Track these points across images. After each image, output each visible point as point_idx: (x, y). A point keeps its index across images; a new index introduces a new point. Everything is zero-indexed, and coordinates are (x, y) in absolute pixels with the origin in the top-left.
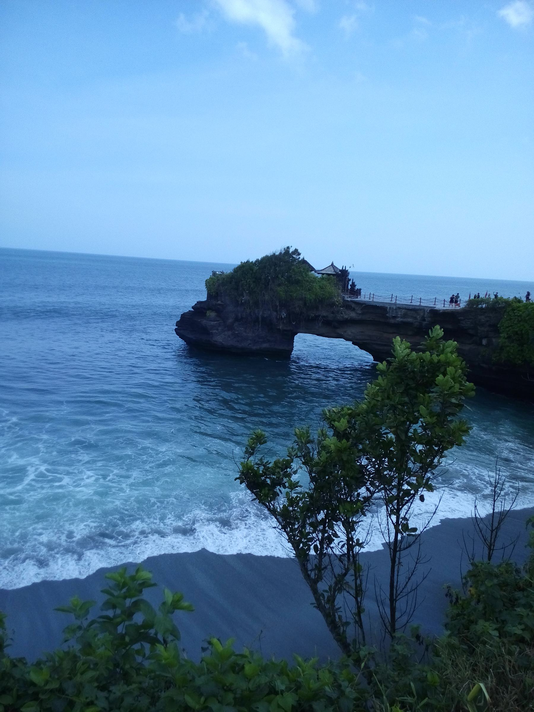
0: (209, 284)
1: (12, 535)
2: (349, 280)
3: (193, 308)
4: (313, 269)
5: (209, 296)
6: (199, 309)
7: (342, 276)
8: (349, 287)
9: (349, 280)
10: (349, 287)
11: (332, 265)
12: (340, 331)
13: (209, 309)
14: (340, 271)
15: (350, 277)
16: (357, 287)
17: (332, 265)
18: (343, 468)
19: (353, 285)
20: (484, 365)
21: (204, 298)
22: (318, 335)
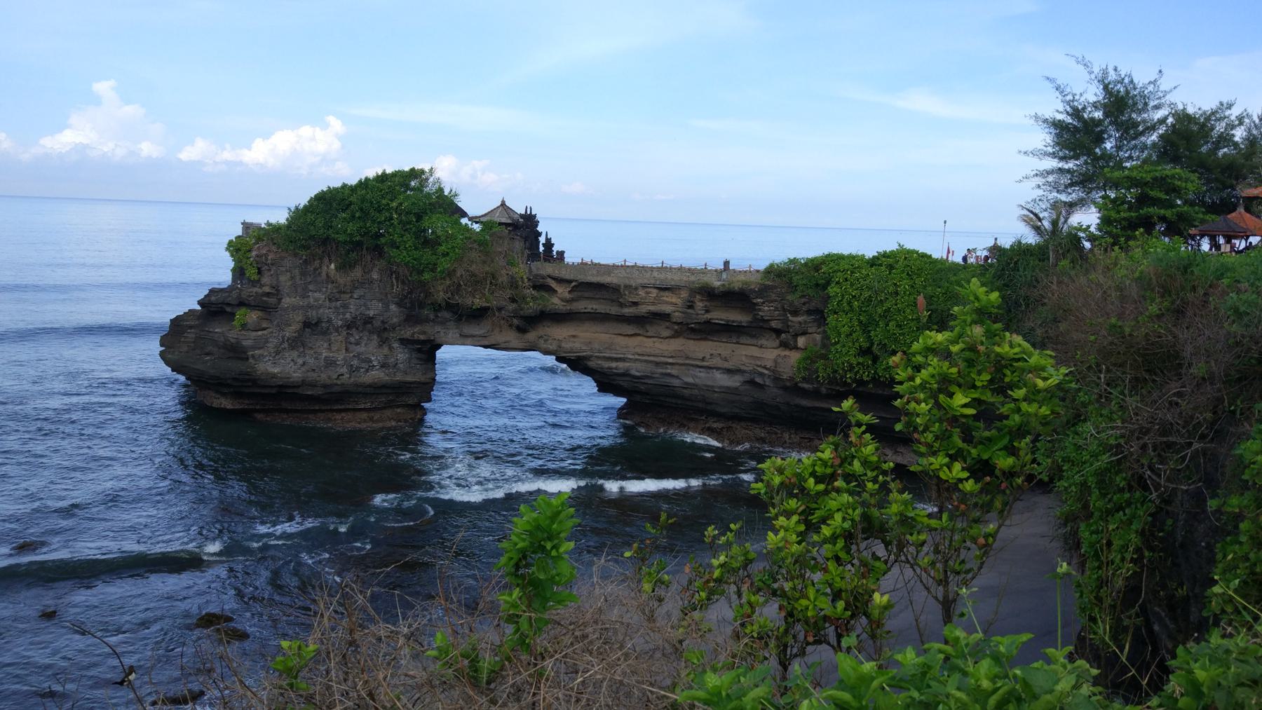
0: (236, 248)
1: (282, 258)
2: (540, 234)
3: (200, 303)
4: (464, 214)
5: (238, 272)
6: (216, 306)
7: (522, 228)
8: (541, 249)
9: (540, 234)
10: (541, 249)
11: (503, 204)
12: (531, 336)
13: (242, 304)
14: (521, 216)
15: (539, 229)
16: (555, 249)
17: (503, 204)
18: (919, 276)
19: (549, 245)
20: (806, 386)
21: (224, 277)
22: (486, 347)
